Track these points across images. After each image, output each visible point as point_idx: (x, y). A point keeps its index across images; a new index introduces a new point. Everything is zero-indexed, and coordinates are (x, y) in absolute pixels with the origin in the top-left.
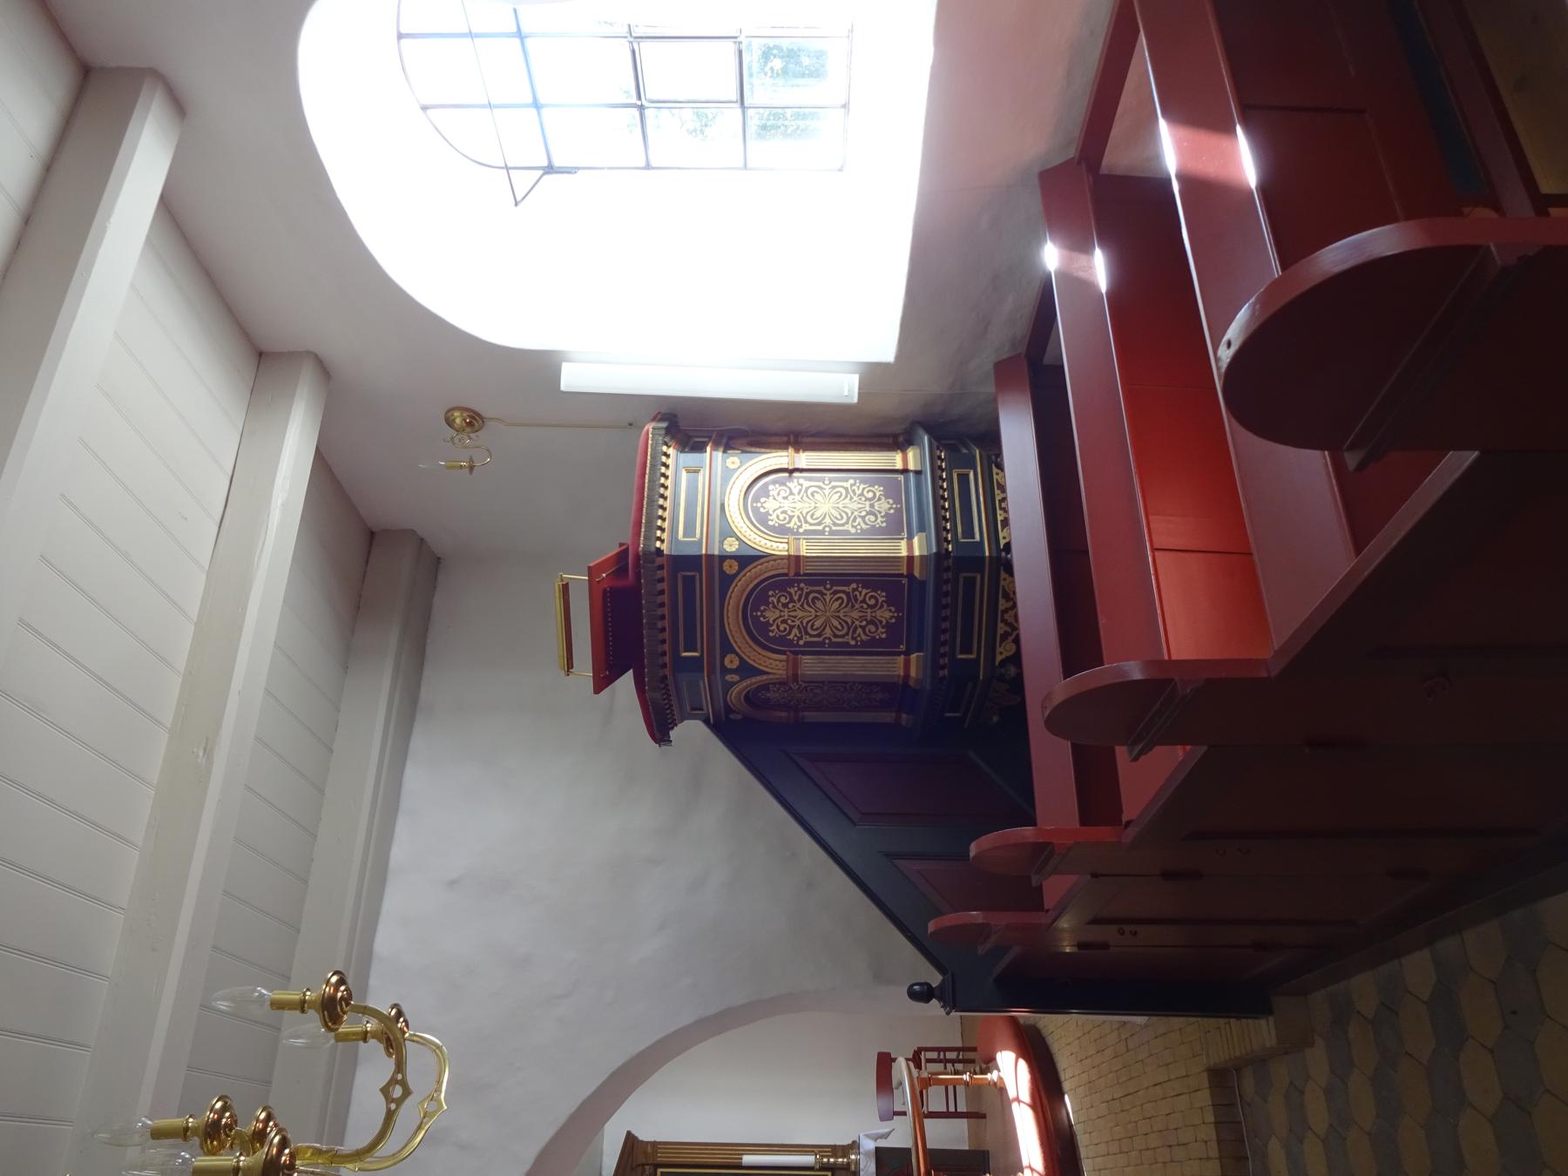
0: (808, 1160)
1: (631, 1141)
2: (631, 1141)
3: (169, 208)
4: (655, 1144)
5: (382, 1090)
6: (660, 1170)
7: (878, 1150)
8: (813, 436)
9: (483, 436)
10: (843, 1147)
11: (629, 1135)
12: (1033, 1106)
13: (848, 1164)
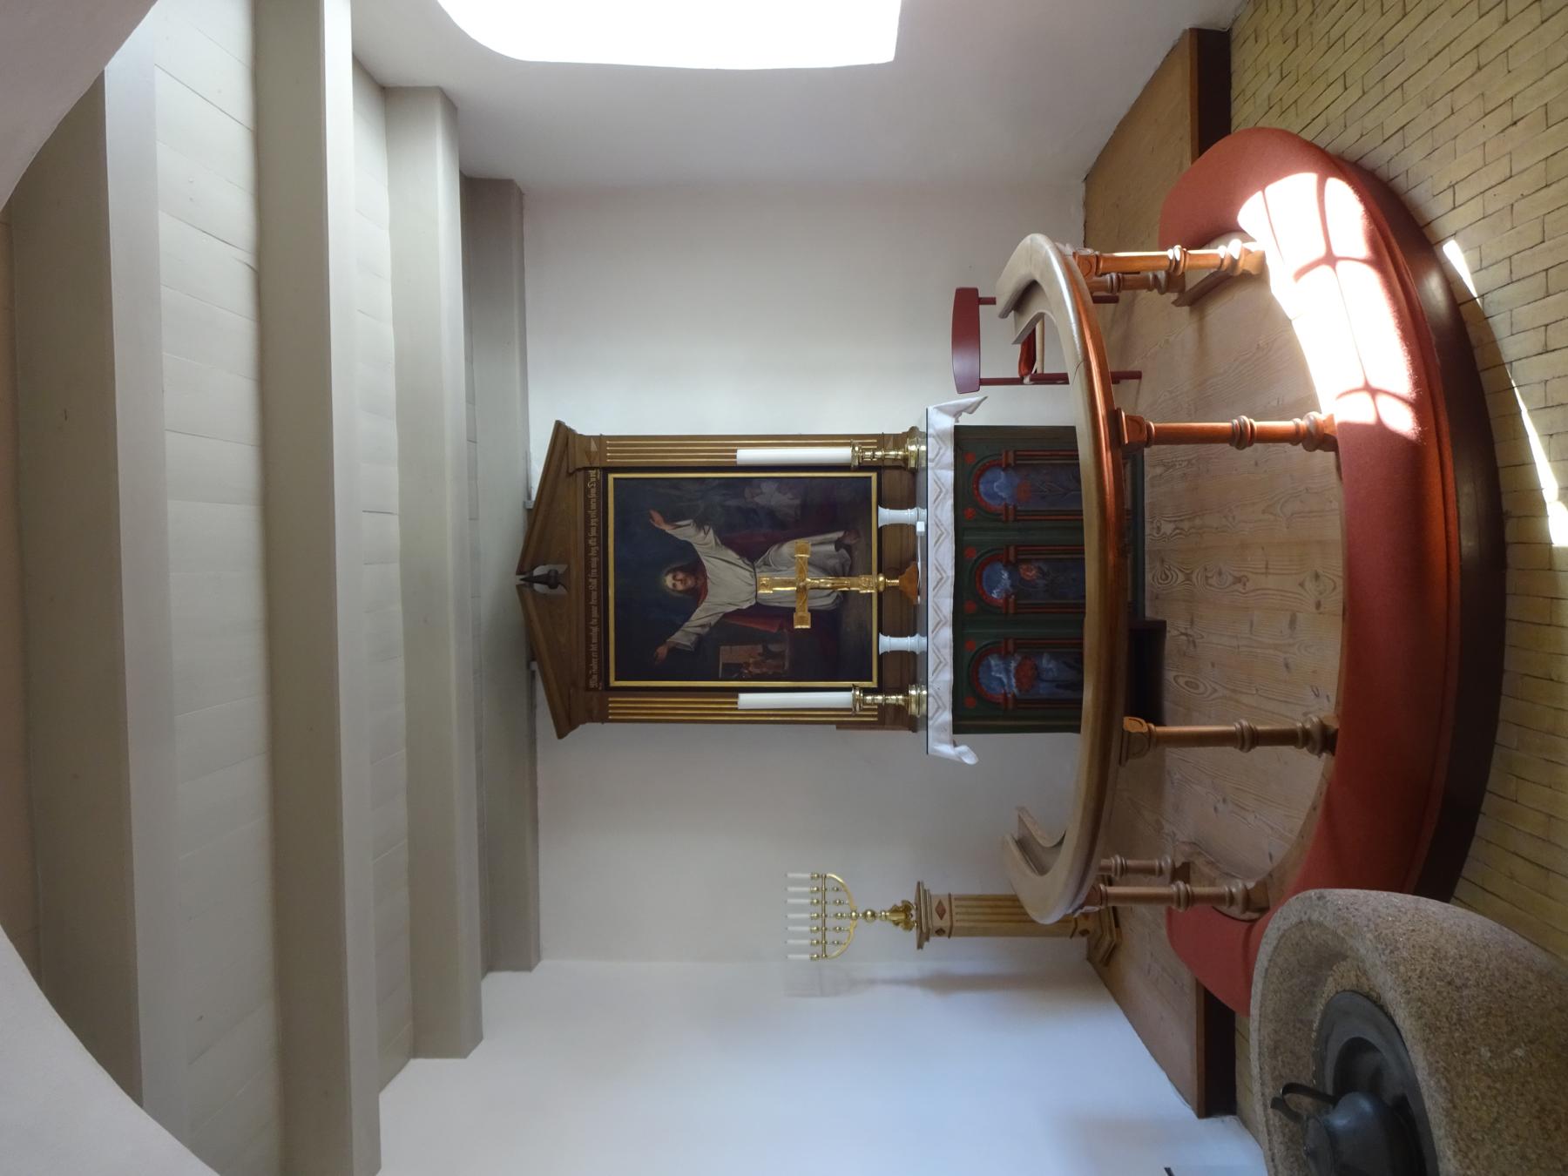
0: (843, 454)
1: (562, 434)
2: (562, 434)
3: (362, 67)
4: (600, 439)
5: (913, 429)
6: (611, 476)
7: (959, 431)
8: (1134, 474)
9: (1320, 572)
10: (896, 436)
11: (560, 428)
12: (1376, 262)
13: (905, 459)
